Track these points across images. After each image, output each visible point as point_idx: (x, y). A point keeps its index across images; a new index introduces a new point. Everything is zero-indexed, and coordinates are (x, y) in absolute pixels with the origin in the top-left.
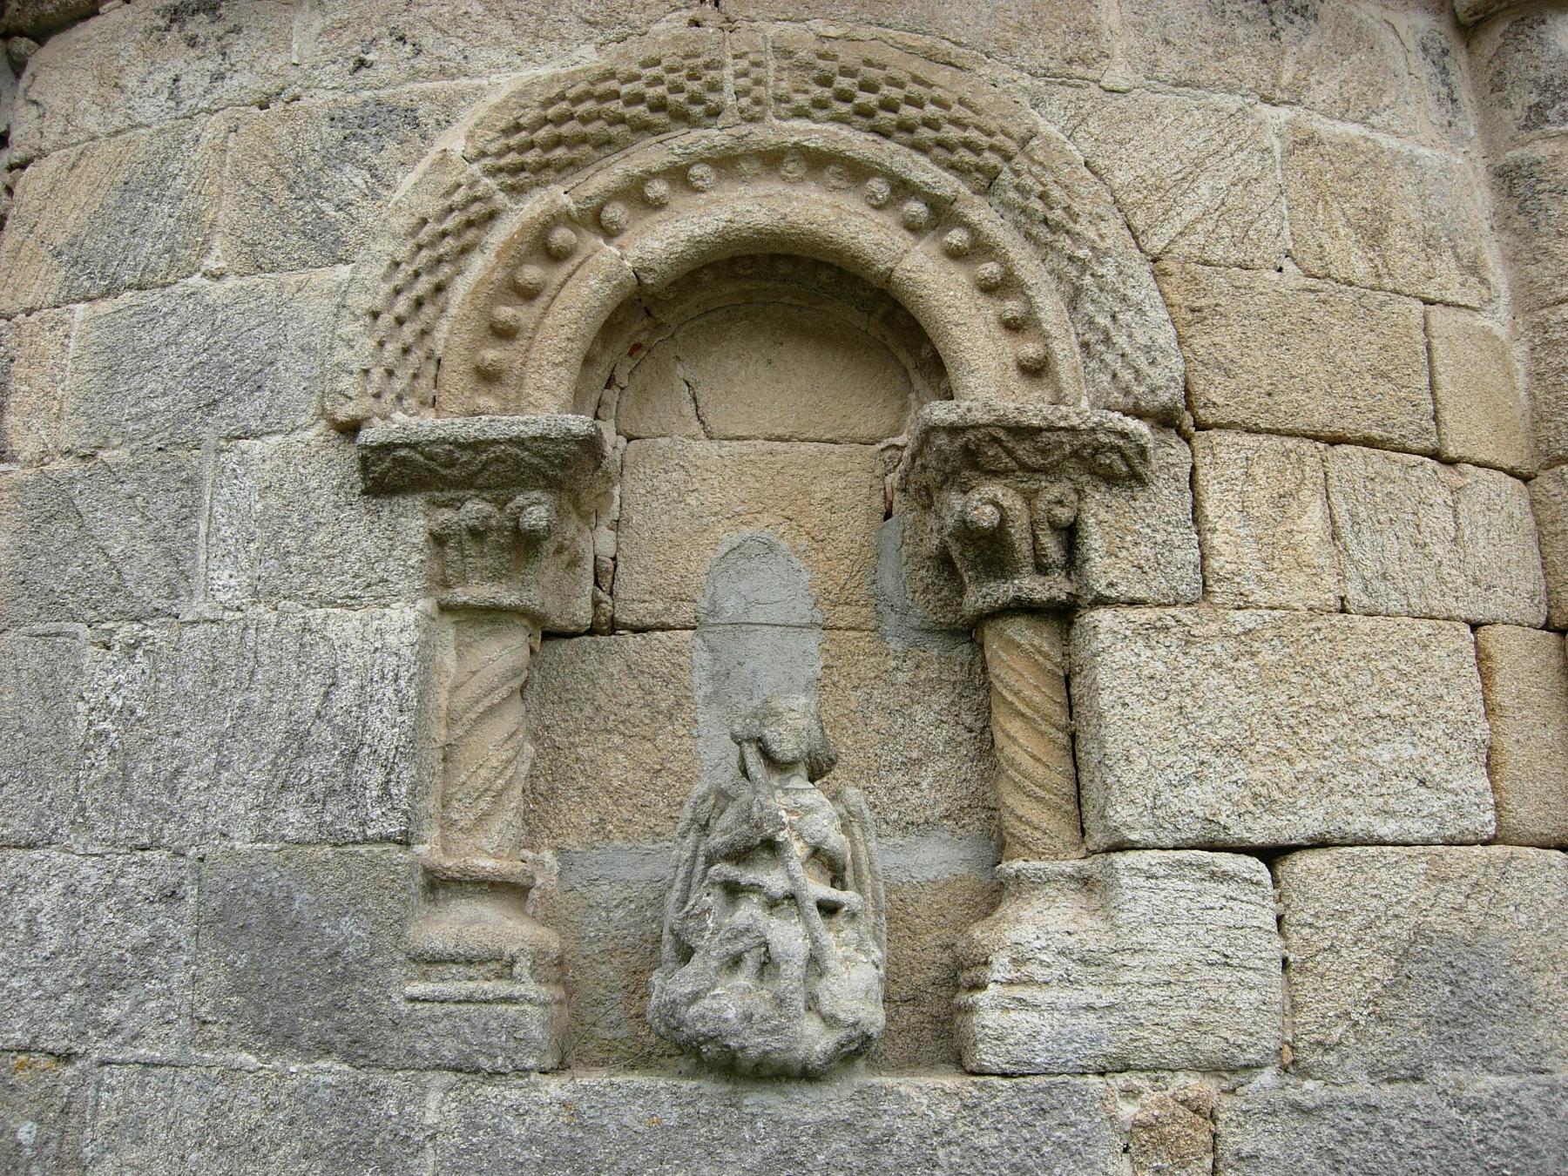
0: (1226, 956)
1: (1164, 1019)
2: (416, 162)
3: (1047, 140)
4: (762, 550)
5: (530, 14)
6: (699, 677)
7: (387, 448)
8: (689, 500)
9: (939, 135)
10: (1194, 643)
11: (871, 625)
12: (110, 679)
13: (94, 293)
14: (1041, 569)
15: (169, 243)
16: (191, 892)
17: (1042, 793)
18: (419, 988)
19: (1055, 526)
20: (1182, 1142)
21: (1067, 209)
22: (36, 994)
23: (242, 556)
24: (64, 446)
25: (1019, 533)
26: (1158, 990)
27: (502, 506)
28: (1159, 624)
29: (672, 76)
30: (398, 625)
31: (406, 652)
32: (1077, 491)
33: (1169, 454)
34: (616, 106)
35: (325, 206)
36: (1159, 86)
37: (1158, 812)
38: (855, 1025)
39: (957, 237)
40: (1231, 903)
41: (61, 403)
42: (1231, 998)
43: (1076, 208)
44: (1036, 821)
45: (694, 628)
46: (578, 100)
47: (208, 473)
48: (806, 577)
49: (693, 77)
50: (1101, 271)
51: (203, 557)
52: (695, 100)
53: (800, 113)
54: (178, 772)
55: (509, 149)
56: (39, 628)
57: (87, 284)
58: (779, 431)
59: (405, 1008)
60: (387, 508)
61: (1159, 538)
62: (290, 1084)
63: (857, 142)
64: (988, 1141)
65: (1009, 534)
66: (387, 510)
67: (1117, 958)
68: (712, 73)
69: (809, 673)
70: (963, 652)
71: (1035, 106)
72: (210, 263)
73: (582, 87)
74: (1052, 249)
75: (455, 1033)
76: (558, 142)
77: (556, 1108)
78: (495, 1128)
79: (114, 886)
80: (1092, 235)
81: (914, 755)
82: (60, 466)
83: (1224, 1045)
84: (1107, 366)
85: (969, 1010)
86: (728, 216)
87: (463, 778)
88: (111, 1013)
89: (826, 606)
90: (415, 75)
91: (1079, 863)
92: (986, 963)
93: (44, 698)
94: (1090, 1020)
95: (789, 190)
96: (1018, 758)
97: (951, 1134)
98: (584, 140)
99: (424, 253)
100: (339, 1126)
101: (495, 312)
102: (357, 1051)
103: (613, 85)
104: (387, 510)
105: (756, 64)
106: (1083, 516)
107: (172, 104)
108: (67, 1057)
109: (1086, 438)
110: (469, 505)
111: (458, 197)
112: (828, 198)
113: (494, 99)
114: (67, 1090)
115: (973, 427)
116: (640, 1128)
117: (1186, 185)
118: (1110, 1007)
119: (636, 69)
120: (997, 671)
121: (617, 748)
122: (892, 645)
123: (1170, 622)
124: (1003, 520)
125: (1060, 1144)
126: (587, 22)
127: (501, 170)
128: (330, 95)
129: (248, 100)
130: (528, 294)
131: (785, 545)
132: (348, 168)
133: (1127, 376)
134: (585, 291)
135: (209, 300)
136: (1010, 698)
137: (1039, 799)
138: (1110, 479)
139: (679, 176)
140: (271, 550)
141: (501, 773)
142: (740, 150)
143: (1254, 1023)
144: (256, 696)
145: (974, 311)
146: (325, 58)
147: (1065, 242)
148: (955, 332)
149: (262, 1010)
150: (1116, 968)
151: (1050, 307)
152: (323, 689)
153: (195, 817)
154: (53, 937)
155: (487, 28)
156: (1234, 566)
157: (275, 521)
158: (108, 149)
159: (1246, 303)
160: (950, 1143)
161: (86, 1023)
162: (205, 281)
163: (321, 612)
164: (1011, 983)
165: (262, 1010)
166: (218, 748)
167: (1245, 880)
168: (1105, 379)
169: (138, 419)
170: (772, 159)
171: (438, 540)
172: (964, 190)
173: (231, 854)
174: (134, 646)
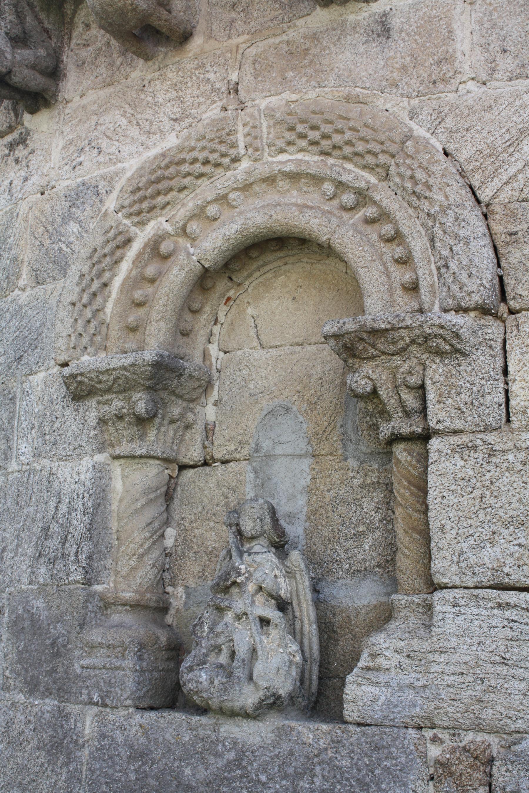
0: (504, 659)
3: (417, 140)
8: (250, 386)
10: (494, 455)
23: (30, 436)
26: (453, 678)
28: (470, 445)
30: (84, 469)
31: (88, 483)
34: (185, 168)
38: (267, 688)
40: (512, 624)
42: (506, 686)
43: (431, 181)
45: (248, 460)
48: (305, 426)
53: (282, 151)
62: (35, 710)
63: (311, 160)
64: (345, 763)
69: (303, 483)
71: (411, 118)
75: (97, 686)
83: (499, 716)
100: (51, 733)
102: (62, 690)
103: (183, 155)
105: (254, 127)
109: (418, 332)
111: (111, 235)
113: (129, 174)
115: (347, 333)
116: (173, 741)
117: (512, 150)
119: (193, 143)
125: (386, 769)
126: (172, 119)
127: (131, 214)
131: (295, 408)
133: (455, 288)
140: (39, 433)
141: (141, 545)
142: (252, 180)
143: (521, 704)
144: (31, 509)
147: (426, 205)
149: (27, 671)
151: (418, 245)
155: (128, 132)
165: (27, 671)
171: (102, 421)
172: (373, 180)
173: (21, 592)
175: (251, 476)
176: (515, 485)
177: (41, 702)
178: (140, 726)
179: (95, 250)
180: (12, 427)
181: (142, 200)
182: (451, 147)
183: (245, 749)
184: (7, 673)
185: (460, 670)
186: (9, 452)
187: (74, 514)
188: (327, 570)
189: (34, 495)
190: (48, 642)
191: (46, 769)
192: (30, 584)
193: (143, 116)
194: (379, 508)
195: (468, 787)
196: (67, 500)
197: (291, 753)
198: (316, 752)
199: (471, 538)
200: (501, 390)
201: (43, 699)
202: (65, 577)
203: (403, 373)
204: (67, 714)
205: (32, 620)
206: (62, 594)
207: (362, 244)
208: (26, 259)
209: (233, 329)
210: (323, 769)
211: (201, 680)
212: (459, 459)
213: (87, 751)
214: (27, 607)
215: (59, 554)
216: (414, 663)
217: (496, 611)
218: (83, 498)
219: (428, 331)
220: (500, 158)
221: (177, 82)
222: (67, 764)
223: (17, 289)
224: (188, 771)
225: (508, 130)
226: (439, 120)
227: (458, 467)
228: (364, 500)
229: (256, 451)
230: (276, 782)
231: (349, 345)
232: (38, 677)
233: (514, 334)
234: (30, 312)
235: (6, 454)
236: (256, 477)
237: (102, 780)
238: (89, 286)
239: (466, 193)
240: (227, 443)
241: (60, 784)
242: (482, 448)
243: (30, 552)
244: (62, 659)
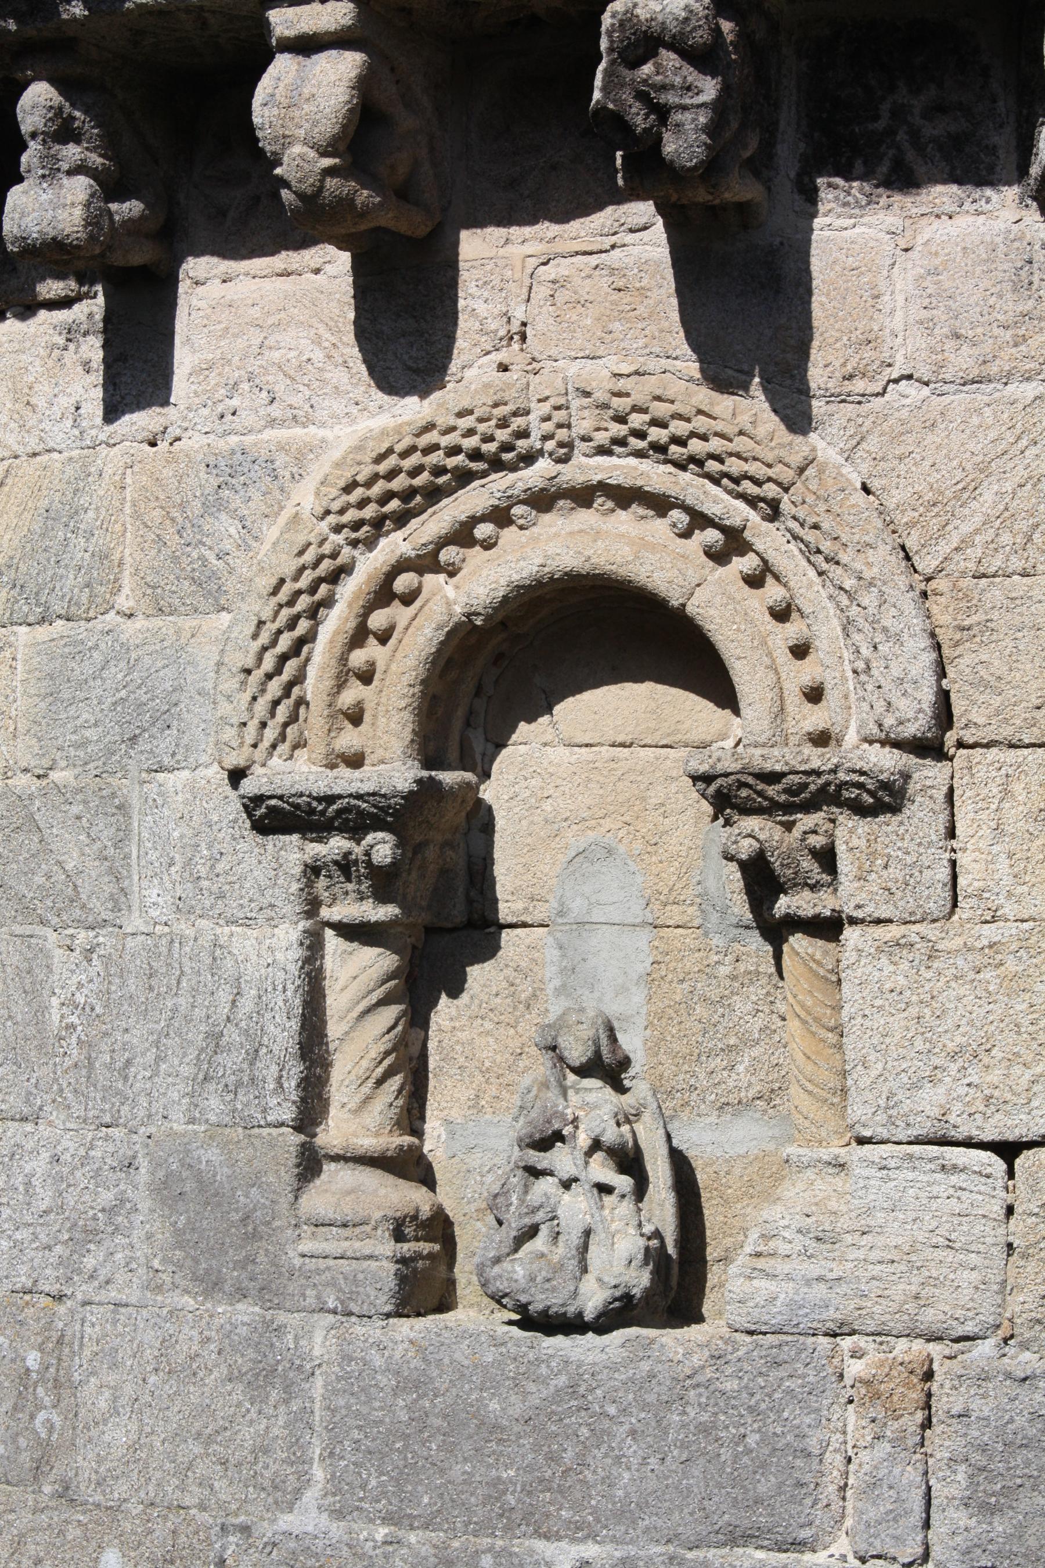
2: (277, 514)
4: (602, 853)
6: (550, 971)
9: (724, 468)
11: (696, 923)
12: (75, 979)
13: (31, 619)
15: (87, 578)
16: (143, 1162)
18: (307, 1246)
22: (34, 1246)
23: (166, 877)
24: (24, 764)
26: (879, 1267)
30: (284, 944)
33: (930, 774)
35: (207, 553)
36: (946, 388)
37: (890, 1112)
40: (959, 1193)
41: (16, 723)
42: (952, 1276)
47: (135, 802)
48: (639, 879)
49: (503, 423)
51: (136, 878)
53: (603, 451)
54: (128, 1063)
56: (18, 929)
57: (26, 609)
58: (620, 739)
59: (297, 1262)
60: (273, 842)
61: (909, 860)
62: (217, 1321)
63: (655, 476)
64: (731, 1385)
66: (271, 843)
72: (123, 602)
73: (407, 442)
75: (333, 1283)
77: (406, 1345)
78: (363, 1359)
79: (86, 1157)
81: (732, 1043)
82: (21, 781)
83: (942, 1317)
86: (538, 561)
88: (89, 1262)
89: (656, 906)
90: (272, 423)
91: (837, 1151)
93: (25, 992)
94: (820, 1290)
97: (699, 1378)
100: (253, 1356)
102: (268, 1292)
103: (432, 437)
104: (271, 843)
107: (76, 432)
108: (59, 1298)
111: (309, 557)
113: (337, 454)
114: (61, 1325)
115: (721, 775)
116: (466, 1363)
117: (965, 495)
119: (452, 421)
121: (488, 1033)
122: (714, 942)
125: (790, 1392)
126: (409, 368)
128: (206, 440)
129: (140, 438)
131: (622, 848)
132: (223, 516)
134: (421, 640)
135: (123, 638)
139: (501, 517)
140: (186, 875)
144: (181, 1001)
149: (197, 1261)
151: (826, 632)
152: (231, 997)
153: (143, 1101)
154: (45, 1199)
156: (981, 884)
157: (188, 849)
158: (28, 468)
159: (1021, 614)
160: (698, 1385)
161: (70, 1269)
162: (119, 619)
163: (227, 930)
164: (758, 1255)
165: (197, 1261)
166: (157, 1044)
167: (975, 1172)
169: (77, 746)
170: (583, 496)
171: (313, 870)
173: (171, 1134)
174: (91, 951)
175: (552, 954)
176: (965, 1001)
177: (229, 1309)
178: (411, 1342)
179: (282, 581)
180: (127, 857)
181: (362, 504)
182: (874, 484)
183: (581, 1371)
184: (156, 1263)
186: (124, 899)
187: (268, 1015)
188: (681, 1102)
189: (184, 980)
190: (235, 1217)
191: (248, 1411)
192: (188, 1123)
194: (758, 1011)
196: (253, 992)
197: (652, 1376)
198: (689, 1373)
200: (946, 863)
201: (231, 1304)
202: (259, 1116)
204: (280, 1327)
205: (200, 1182)
206: (257, 1142)
207: (737, 620)
208: (128, 560)
210: (700, 1395)
211: (515, 1277)
213: (319, 1381)
214: (188, 1160)
215: (246, 1079)
216: (824, 1246)
217: (939, 1176)
218: (285, 990)
222: (286, 1402)
223: (112, 613)
224: (494, 1405)
226: (858, 438)
227: (886, 973)
228: (735, 998)
229: (561, 913)
230: (631, 1415)
232: (220, 1271)
233: (965, 781)
234: (147, 660)
235: (116, 902)
236: (564, 956)
237: (351, 1422)
238: (274, 643)
239: (896, 559)
241: (276, 1431)
243: (186, 1070)
244: (264, 1243)
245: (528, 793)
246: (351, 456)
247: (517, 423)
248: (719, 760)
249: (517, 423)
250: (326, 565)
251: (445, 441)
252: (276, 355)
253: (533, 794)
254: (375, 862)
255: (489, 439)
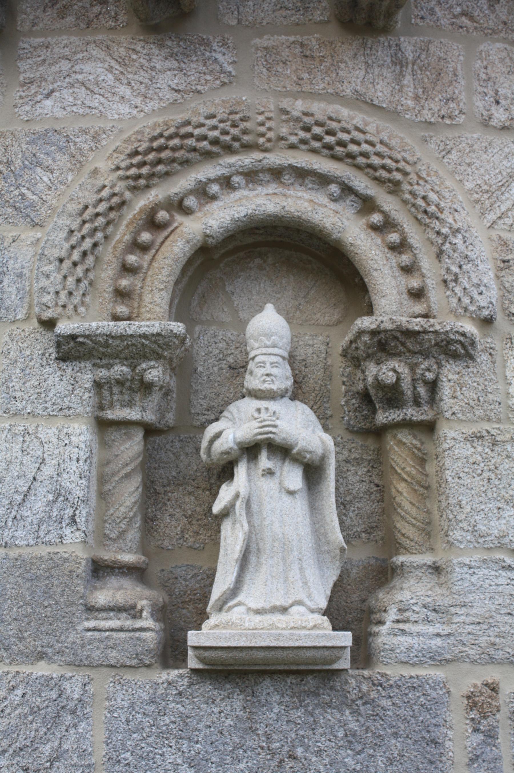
1: (477, 642)
5: (141, 83)
7: (73, 337)
8: (228, 359)
9: (369, 162)
10: (497, 445)
14: (417, 403)
17: (414, 522)
19: (426, 383)
20: (485, 706)
21: (437, 206)
25: (406, 385)
27: (133, 367)
29: (222, 125)
31: (83, 446)
32: (437, 363)
34: (191, 142)
39: (376, 218)
43: (442, 204)
44: (412, 537)
46: (170, 137)
50: (454, 241)
52: (235, 139)
55: (132, 165)
60: (69, 369)
65: (401, 386)
67: (453, 610)
68: (245, 124)
70: (371, 443)
73: (172, 130)
74: (428, 227)
76: (160, 161)
80: (450, 220)
83: (507, 656)
84: (456, 294)
85: (377, 634)
86: (254, 207)
87: (111, 511)
92: (385, 611)
94: (438, 641)
95: (285, 191)
96: (403, 504)
98: (173, 160)
99: (87, 226)
101: (126, 259)
103: (189, 129)
104: (70, 369)
106: (440, 376)
110: (116, 368)
111: (105, 193)
112: (307, 195)
117: (503, 189)
118: (449, 635)
119: (202, 120)
120: (393, 457)
123: (485, 433)
124: (398, 379)
127: (127, 178)
130: (144, 248)
132: (39, 170)
136: (399, 471)
137: (414, 525)
138: (455, 356)
139: (226, 183)
145: (385, 262)
146: (21, 101)
147: (436, 225)
148: (375, 274)
150: (453, 615)
151: (426, 262)
164: (398, 621)
168: (455, 300)
170: (277, 173)
171: (98, 385)
179: (86, 207)
181: (141, 165)
185: (477, 620)
187: (65, 476)
193: (136, 77)
195: (490, 714)
199: (482, 512)
203: (423, 369)
209: (206, 302)
212: (470, 446)
219: (452, 337)
220: (494, 195)
221: (178, 52)
225: (500, 172)
231: (383, 341)
240: (206, 412)
242: (487, 438)
245: (218, 351)
246: (134, 136)
247: (243, 125)
248: (382, 322)
249: (243, 125)
250: (115, 200)
251: (197, 132)
252: (80, 77)
253: (221, 352)
254: (145, 380)
255: (225, 133)
